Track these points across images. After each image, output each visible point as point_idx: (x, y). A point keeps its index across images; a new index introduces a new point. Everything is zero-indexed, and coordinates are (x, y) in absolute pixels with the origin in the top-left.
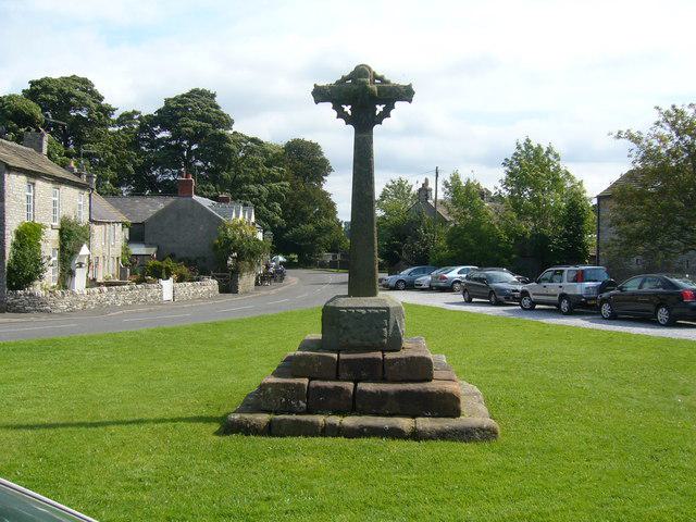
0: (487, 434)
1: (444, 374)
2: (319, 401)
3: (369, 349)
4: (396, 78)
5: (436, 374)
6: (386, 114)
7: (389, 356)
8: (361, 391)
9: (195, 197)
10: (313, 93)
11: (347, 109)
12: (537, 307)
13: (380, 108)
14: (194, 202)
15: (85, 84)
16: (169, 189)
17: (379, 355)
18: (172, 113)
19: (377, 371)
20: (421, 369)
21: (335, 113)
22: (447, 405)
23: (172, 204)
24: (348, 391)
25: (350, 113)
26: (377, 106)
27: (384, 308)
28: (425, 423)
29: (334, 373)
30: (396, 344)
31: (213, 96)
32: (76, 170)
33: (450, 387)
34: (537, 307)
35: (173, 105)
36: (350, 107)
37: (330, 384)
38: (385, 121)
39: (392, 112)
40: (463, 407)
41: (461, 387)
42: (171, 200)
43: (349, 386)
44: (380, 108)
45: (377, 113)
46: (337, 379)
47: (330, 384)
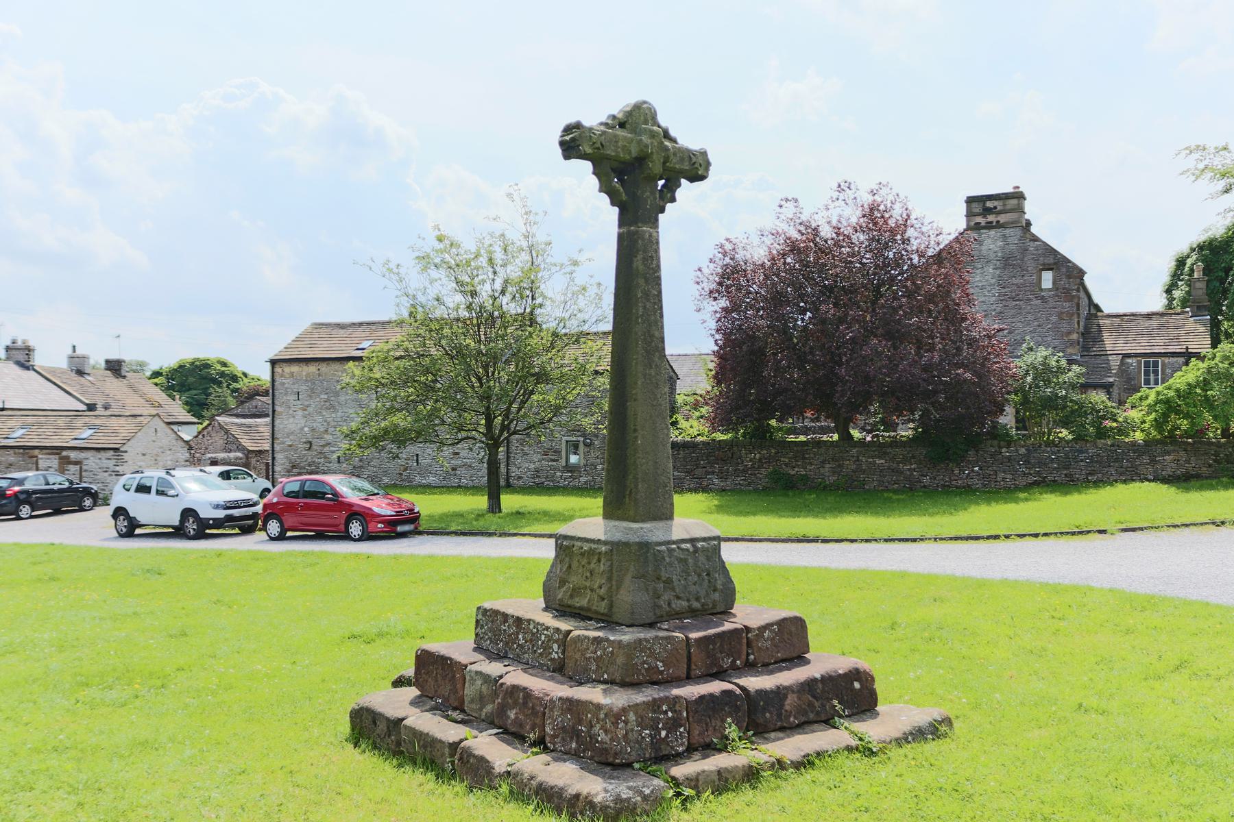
4: (687, 138)
12: (138, 531)
20: (789, 639)
34: (289, 534)
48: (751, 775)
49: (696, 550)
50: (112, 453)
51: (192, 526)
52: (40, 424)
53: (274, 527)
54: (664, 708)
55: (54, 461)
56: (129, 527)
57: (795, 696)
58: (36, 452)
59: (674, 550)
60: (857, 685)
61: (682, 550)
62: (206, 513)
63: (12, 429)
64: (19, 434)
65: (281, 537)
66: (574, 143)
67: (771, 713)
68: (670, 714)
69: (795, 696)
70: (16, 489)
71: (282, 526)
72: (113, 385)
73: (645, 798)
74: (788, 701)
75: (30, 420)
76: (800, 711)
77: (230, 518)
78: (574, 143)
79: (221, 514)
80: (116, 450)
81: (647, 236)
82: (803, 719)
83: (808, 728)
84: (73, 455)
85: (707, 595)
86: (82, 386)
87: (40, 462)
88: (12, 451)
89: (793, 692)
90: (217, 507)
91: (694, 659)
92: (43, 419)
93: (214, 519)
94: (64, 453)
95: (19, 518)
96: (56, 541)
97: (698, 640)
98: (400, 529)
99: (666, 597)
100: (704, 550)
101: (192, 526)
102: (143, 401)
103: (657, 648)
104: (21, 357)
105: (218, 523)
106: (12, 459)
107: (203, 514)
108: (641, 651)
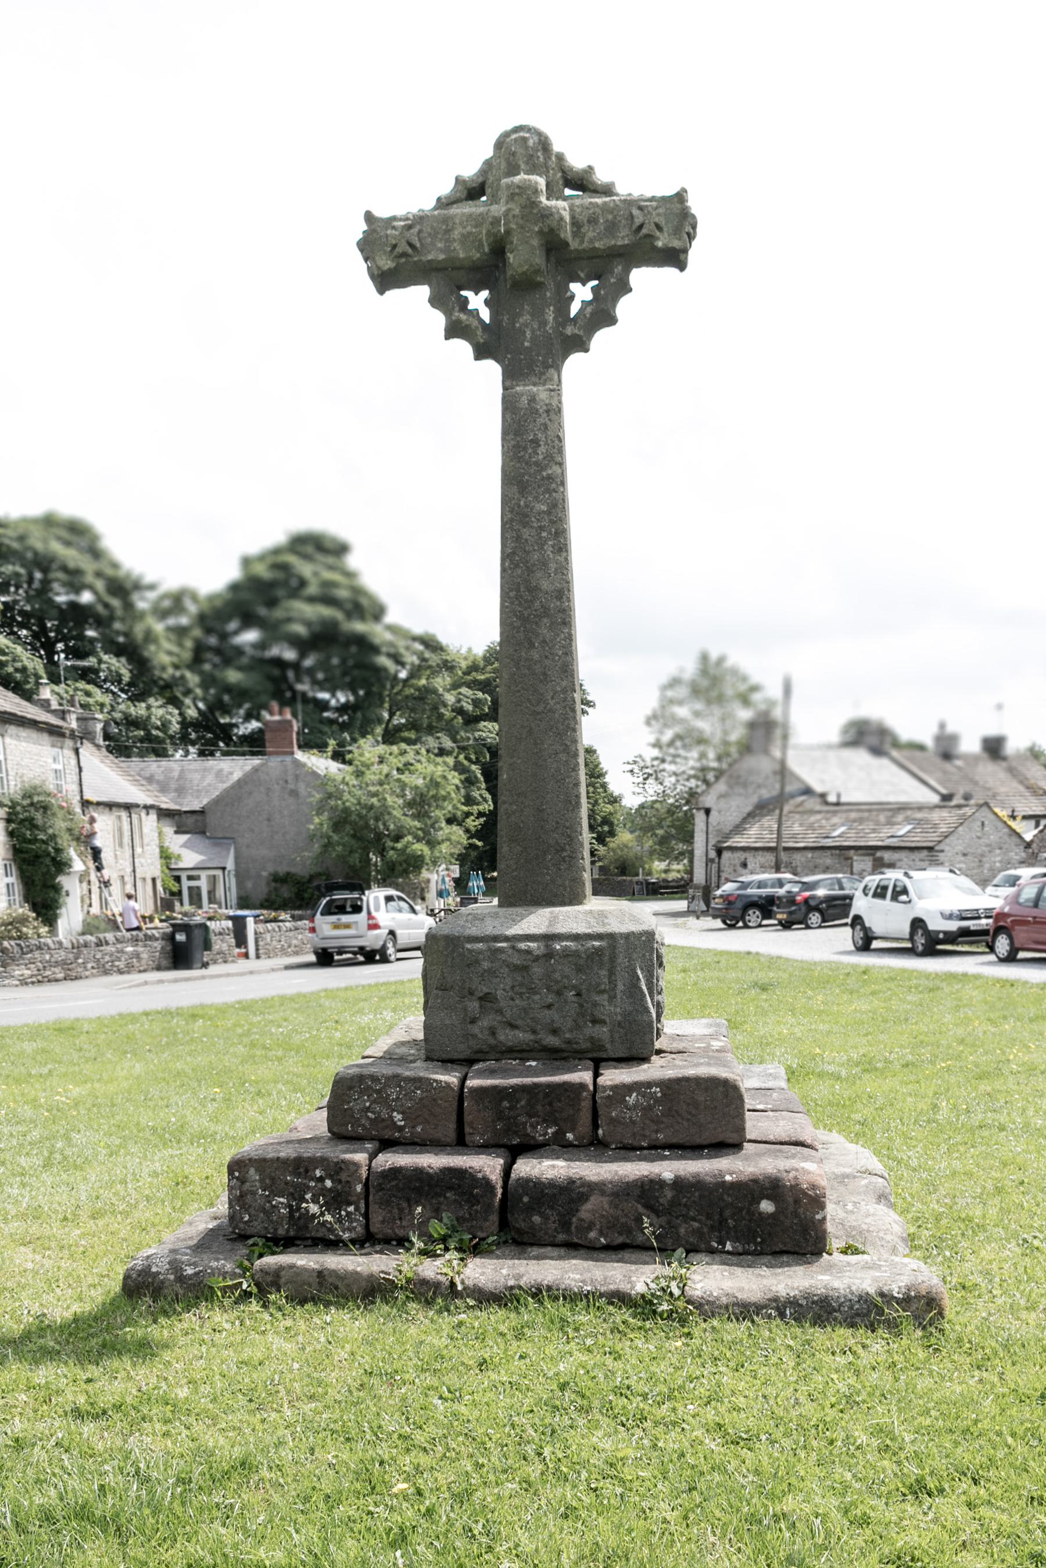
0: (924, 1309)
1: (780, 1127)
2: (388, 1212)
3: (559, 1056)
4: (634, 175)
5: (754, 1126)
6: (602, 315)
7: (613, 1076)
8: (526, 1183)
9: (300, 755)
10: (368, 246)
11: (478, 301)
12: (1021, 955)
13: (582, 292)
14: (298, 764)
15: (77, 531)
16: (255, 744)
17: (585, 1076)
18: (260, 592)
19: (593, 1128)
20: (708, 1112)
21: (438, 320)
22: (781, 1224)
23: (255, 770)
24: (487, 1185)
25: (485, 315)
26: (575, 287)
27: (599, 937)
28: (712, 1279)
29: (449, 1130)
30: (637, 1043)
31: (341, 549)
32: (54, 705)
33: (805, 1169)
34: (1021, 955)
35: (261, 570)
36: (485, 294)
37: (432, 1161)
38: (601, 338)
39: (624, 307)
40: (837, 1216)
41: (838, 1166)
42: (256, 761)
43: (488, 1165)
44: (582, 292)
45: (575, 308)
46: (461, 1143)
47: (432, 1161)
48: (425, 1292)
49: (550, 955)
50: (925, 853)
51: (927, 942)
52: (861, 821)
53: (1002, 944)
54: (318, 1173)
55: (867, 863)
56: (865, 943)
57: (605, 1200)
58: (852, 852)
59: (501, 950)
60: (766, 1206)
61: (519, 951)
62: (936, 924)
63: (834, 827)
64: (839, 832)
65: (1011, 958)
66: (395, 256)
67: (545, 1218)
68: (328, 1183)
69: (605, 1200)
70: (807, 894)
71: (1012, 943)
72: (990, 773)
73: (181, 1279)
74: (588, 1206)
75: (853, 815)
76: (611, 1225)
77: (965, 932)
78: (395, 256)
79: (953, 926)
80: (930, 849)
81: (524, 400)
82: (620, 1240)
83: (626, 1254)
84: (887, 856)
85: (577, 1027)
86: (945, 772)
87: (855, 864)
88: (829, 852)
89: (603, 1193)
90: (950, 917)
91: (468, 1118)
92: (866, 814)
93: (945, 933)
94: (879, 854)
95: (808, 927)
96: (753, 950)
97: (481, 1092)
98: (940, 947)
99: (485, 1023)
100: (566, 954)
101: (927, 942)
102: (1021, 788)
103: (393, 1093)
104: (873, 740)
105: (951, 938)
106: (828, 861)
107: (931, 927)
108: (362, 1093)
